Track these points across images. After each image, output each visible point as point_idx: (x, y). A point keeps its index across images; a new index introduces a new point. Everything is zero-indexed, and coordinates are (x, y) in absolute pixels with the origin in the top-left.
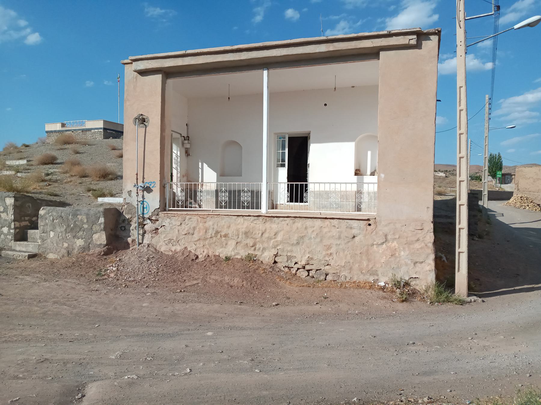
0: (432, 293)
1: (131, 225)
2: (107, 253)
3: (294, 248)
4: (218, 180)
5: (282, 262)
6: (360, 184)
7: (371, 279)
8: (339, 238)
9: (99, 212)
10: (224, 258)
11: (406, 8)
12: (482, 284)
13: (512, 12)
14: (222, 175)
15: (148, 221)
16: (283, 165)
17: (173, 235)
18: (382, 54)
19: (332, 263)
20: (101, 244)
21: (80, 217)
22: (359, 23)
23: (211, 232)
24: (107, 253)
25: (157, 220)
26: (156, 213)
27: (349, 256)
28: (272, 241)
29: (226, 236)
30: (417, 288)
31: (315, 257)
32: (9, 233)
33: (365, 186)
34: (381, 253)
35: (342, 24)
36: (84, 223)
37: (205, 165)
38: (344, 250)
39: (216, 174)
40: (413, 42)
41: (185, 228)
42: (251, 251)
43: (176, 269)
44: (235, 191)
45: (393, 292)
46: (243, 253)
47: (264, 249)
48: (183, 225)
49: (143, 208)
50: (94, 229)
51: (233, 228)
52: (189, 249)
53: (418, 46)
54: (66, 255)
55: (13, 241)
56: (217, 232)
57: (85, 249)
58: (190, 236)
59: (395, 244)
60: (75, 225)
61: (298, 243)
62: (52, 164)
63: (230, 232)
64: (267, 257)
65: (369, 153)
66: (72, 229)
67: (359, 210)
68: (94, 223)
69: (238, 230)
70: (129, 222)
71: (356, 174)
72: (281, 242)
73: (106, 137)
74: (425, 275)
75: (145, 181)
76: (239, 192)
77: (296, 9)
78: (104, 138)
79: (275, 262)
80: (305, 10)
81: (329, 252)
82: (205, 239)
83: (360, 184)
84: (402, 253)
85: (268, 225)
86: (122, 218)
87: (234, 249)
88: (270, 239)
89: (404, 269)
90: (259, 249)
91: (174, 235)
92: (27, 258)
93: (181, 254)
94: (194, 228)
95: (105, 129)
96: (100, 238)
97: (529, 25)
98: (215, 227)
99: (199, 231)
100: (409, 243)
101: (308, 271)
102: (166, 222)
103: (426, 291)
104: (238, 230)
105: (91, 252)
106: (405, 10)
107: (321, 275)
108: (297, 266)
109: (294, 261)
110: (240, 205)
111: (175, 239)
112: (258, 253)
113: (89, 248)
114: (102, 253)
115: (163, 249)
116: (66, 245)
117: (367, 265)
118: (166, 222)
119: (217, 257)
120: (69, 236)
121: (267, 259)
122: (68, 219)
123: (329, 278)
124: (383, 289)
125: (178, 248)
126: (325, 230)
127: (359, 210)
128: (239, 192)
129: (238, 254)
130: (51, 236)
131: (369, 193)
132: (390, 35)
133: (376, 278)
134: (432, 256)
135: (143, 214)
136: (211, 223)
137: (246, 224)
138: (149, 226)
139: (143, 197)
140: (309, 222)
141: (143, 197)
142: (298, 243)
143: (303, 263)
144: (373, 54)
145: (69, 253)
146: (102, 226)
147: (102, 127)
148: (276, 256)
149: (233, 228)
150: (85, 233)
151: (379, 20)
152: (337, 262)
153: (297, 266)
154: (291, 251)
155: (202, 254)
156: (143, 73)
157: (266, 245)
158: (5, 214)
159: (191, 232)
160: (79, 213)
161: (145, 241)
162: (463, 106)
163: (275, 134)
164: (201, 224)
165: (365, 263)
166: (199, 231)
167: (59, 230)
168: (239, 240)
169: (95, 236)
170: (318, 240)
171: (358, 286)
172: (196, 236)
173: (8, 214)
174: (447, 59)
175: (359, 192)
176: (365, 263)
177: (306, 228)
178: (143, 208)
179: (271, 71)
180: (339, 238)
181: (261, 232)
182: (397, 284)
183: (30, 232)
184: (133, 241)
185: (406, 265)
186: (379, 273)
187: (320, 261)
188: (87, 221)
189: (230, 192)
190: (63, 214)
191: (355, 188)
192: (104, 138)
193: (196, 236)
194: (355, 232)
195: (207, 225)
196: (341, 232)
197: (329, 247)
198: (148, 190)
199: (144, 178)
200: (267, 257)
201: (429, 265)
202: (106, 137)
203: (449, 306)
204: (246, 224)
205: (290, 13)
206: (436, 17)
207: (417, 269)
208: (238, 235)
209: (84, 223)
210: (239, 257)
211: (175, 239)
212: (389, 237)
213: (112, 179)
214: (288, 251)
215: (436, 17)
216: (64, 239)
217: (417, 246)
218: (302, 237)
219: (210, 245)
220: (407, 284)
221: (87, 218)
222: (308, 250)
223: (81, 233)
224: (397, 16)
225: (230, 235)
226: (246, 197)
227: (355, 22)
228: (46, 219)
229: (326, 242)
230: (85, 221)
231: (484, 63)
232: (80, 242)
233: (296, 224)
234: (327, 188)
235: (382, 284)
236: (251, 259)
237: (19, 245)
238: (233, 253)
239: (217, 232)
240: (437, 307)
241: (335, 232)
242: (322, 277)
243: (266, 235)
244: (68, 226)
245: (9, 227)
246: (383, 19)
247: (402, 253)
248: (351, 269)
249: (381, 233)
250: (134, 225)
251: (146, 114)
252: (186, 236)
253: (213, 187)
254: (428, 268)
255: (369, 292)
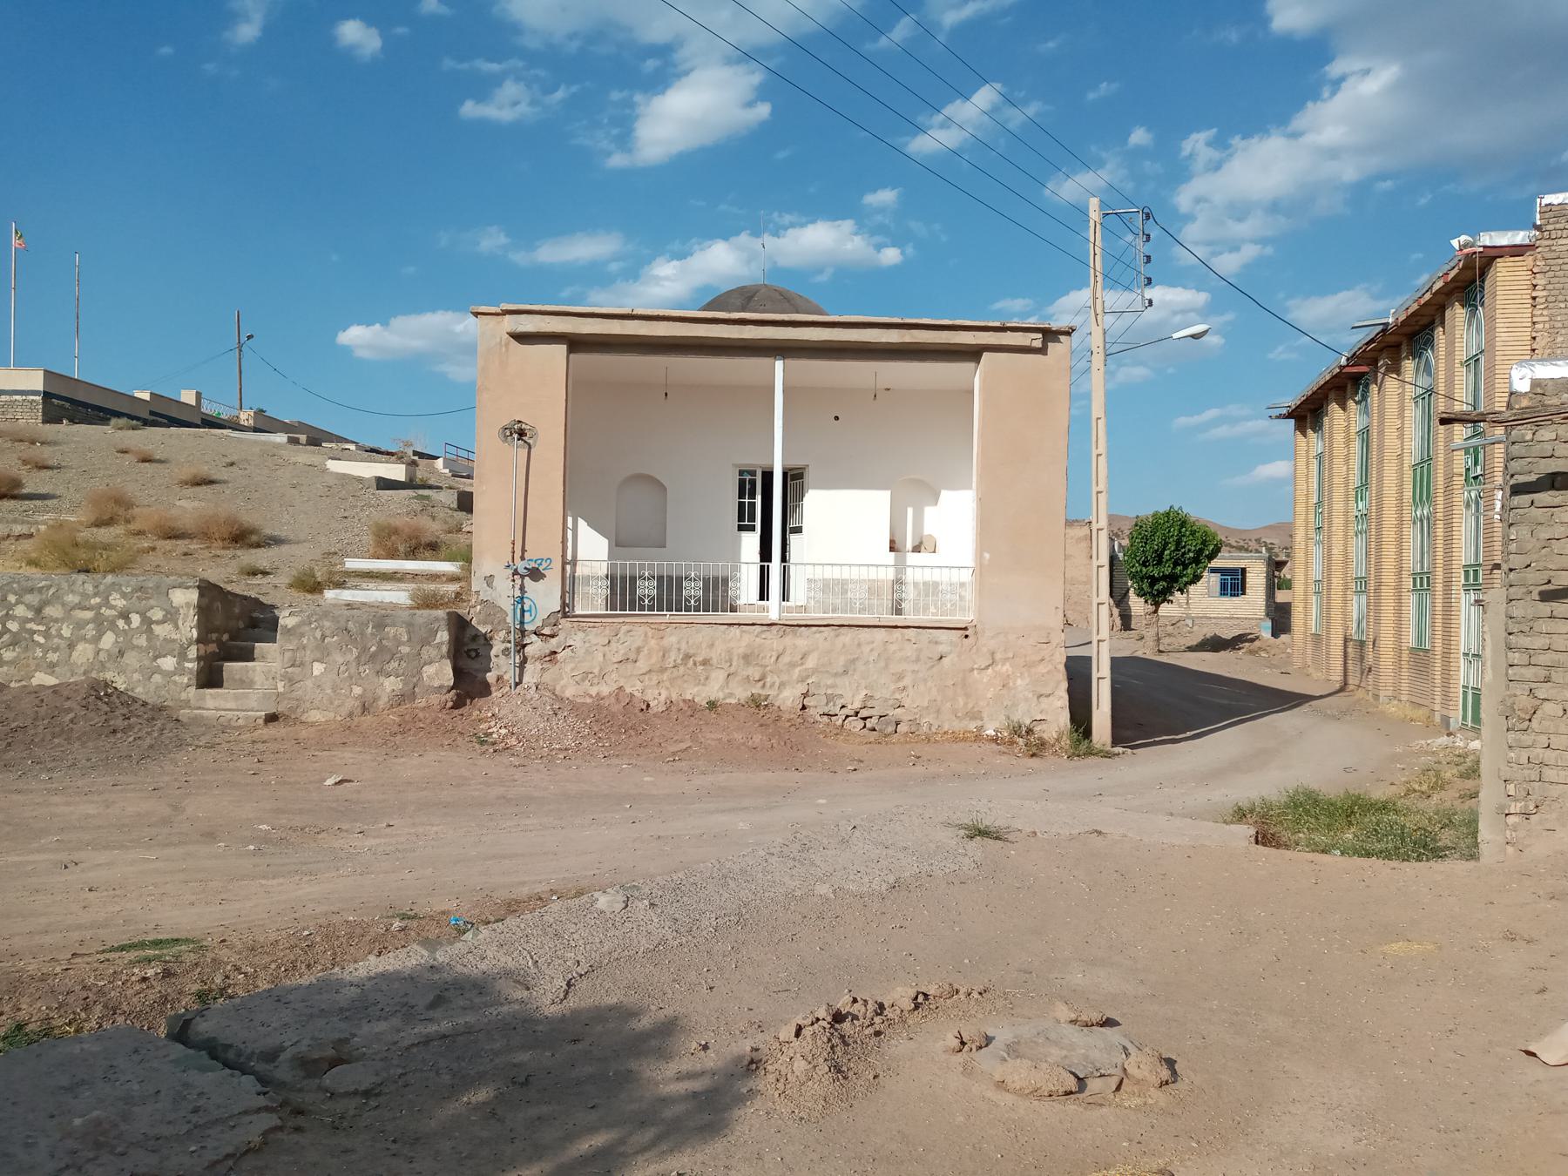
0: (1066, 742)
1: (491, 647)
2: (458, 704)
3: (839, 681)
4: (612, 555)
5: (817, 706)
6: (900, 566)
7: (972, 726)
8: (918, 660)
9: (437, 619)
10: (704, 703)
11: (687, 73)
12: (1129, 730)
13: (942, 126)
14: (618, 544)
15: (534, 638)
16: (753, 529)
17: (595, 663)
18: (986, 356)
19: (907, 702)
20: (441, 687)
21: (391, 631)
22: (560, 94)
23: (673, 657)
24: (458, 704)
25: (552, 636)
26: (553, 621)
27: (934, 691)
28: (797, 670)
29: (705, 662)
30: (1045, 736)
31: (877, 696)
32: (179, 670)
33: (909, 570)
34: (985, 681)
35: (510, 89)
36: (400, 643)
37: (582, 523)
38: (925, 680)
39: (606, 541)
40: (1038, 344)
41: (619, 650)
42: (756, 690)
43: (621, 724)
44: (716, 579)
45: (1012, 743)
46: (741, 693)
47: (782, 685)
48: (613, 644)
49: (523, 611)
50: (425, 656)
51: (720, 648)
52: (628, 690)
53: (1042, 351)
54: (359, 710)
55: (193, 689)
56: (687, 657)
57: (404, 697)
58: (630, 666)
59: (1007, 668)
60: (381, 648)
61: (846, 672)
62: (14, 497)
63: (714, 656)
64: (788, 698)
65: (910, 511)
66: (373, 657)
67: (899, 612)
68: (425, 642)
69: (729, 652)
70: (487, 641)
71: (892, 549)
72: (815, 671)
73: (51, 417)
74: (1056, 716)
75: (527, 555)
76: (680, 580)
77: (369, 20)
78: (44, 422)
79: (804, 708)
80: (401, 30)
81: (901, 685)
82: (663, 670)
83: (900, 566)
84: (1019, 682)
85: (788, 640)
86: (469, 633)
87: (722, 688)
88: (792, 665)
89: (1022, 707)
90: (772, 685)
91: (605, 659)
92: (261, 721)
93: (613, 700)
94: (639, 650)
95: (47, 396)
96: (440, 673)
97: (1193, 336)
98: (684, 646)
99: (649, 656)
100: (1029, 666)
101: (864, 719)
102: (577, 639)
103: (1057, 740)
104: (729, 652)
105: (421, 702)
106: (684, 80)
107: (887, 724)
108: (845, 711)
109: (840, 703)
110: (679, 605)
111: (596, 671)
112: (772, 693)
113: (413, 696)
114: (450, 704)
115: (568, 693)
116: (357, 690)
117: (966, 704)
118: (577, 639)
119: (690, 703)
120: (367, 670)
121: (789, 703)
122: (362, 634)
123: (902, 728)
124: (995, 740)
125: (605, 690)
126: (893, 648)
127: (899, 612)
128: (680, 580)
129: (731, 695)
130: (316, 673)
131: (916, 584)
132: (1003, 329)
133: (979, 723)
134: (1065, 685)
135: (522, 623)
136: (673, 639)
137: (746, 639)
138: (535, 647)
139: (522, 588)
140: (865, 633)
141: (522, 588)
142: (846, 672)
143: (857, 705)
144: (973, 354)
145: (365, 709)
146: (445, 649)
147: (41, 388)
148: (805, 695)
149: (720, 648)
150: (404, 664)
151: (616, 96)
152: (915, 700)
153: (845, 711)
154: (833, 686)
155: (657, 698)
156: (522, 338)
157: (785, 678)
158: (168, 627)
159: (632, 656)
160: (388, 621)
161: (525, 680)
162: (1102, 449)
163: (735, 465)
164: (653, 642)
165: (961, 701)
166: (649, 656)
167: (340, 659)
168: (732, 669)
169: (429, 670)
170: (882, 664)
171: (956, 738)
172: (642, 665)
173: (177, 628)
174: (792, 226)
175: (899, 581)
176: (961, 701)
177: (859, 645)
178: (523, 611)
179: (790, 362)
180: (918, 660)
181: (775, 655)
182: (1016, 730)
183: (230, 667)
184: (499, 678)
185: (1026, 700)
186: (985, 715)
187: (886, 700)
188: (410, 639)
189: (660, 578)
190: (351, 625)
191: (890, 574)
192: (44, 422)
193: (642, 665)
194: (942, 649)
195: (665, 642)
196: (919, 650)
197: (900, 677)
198: (536, 575)
199: (524, 550)
200: (788, 698)
201: (1061, 700)
202: (51, 417)
203: (1091, 760)
204: (746, 639)
205: (352, 32)
206: (763, 110)
207: (1043, 706)
208: (731, 660)
209: (400, 643)
210: (733, 701)
211: (596, 671)
212: (998, 656)
213: (258, 546)
214: (828, 687)
215: (763, 110)
216: (353, 679)
217: (1042, 669)
218: (853, 661)
219: (672, 680)
220: (1030, 731)
221: (409, 633)
222: (863, 683)
223: (394, 664)
224: (663, 92)
225: (714, 661)
226: (692, 590)
227: (549, 90)
228: (302, 635)
229: (896, 668)
230: (405, 638)
231: (879, 247)
232: (391, 685)
233: (842, 638)
234: (846, 574)
235: (991, 732)
236: (756, 703)
237: (213, 697)
238: (721, 695)
239: (687, 657)
240: (1077, 761)
241: (910, 651)
242: (890, 729)
243: (786, 659)
244: (365, 649)
245: (182, 656)
246: (625, 94)
247: (1019, 682)
248: (938, 711)
249: (985, 650)
250: (497, 648)
251: (529, 421)
252: (622, 667)
253: (603, 569)
254: (1059, 704)
255: (975, 746)
